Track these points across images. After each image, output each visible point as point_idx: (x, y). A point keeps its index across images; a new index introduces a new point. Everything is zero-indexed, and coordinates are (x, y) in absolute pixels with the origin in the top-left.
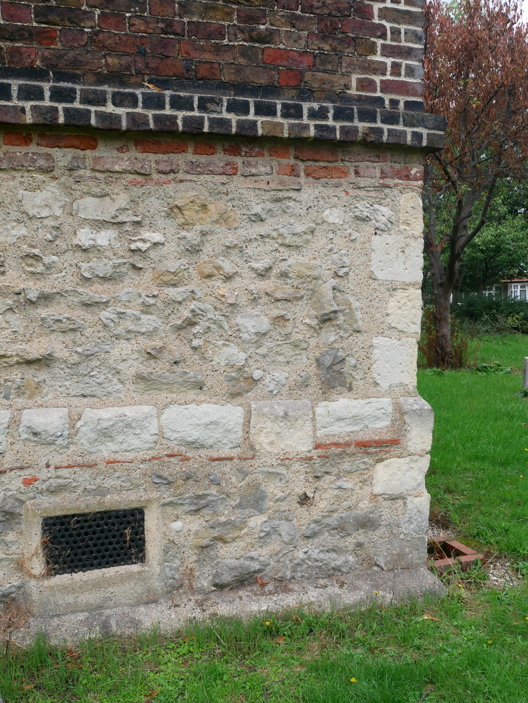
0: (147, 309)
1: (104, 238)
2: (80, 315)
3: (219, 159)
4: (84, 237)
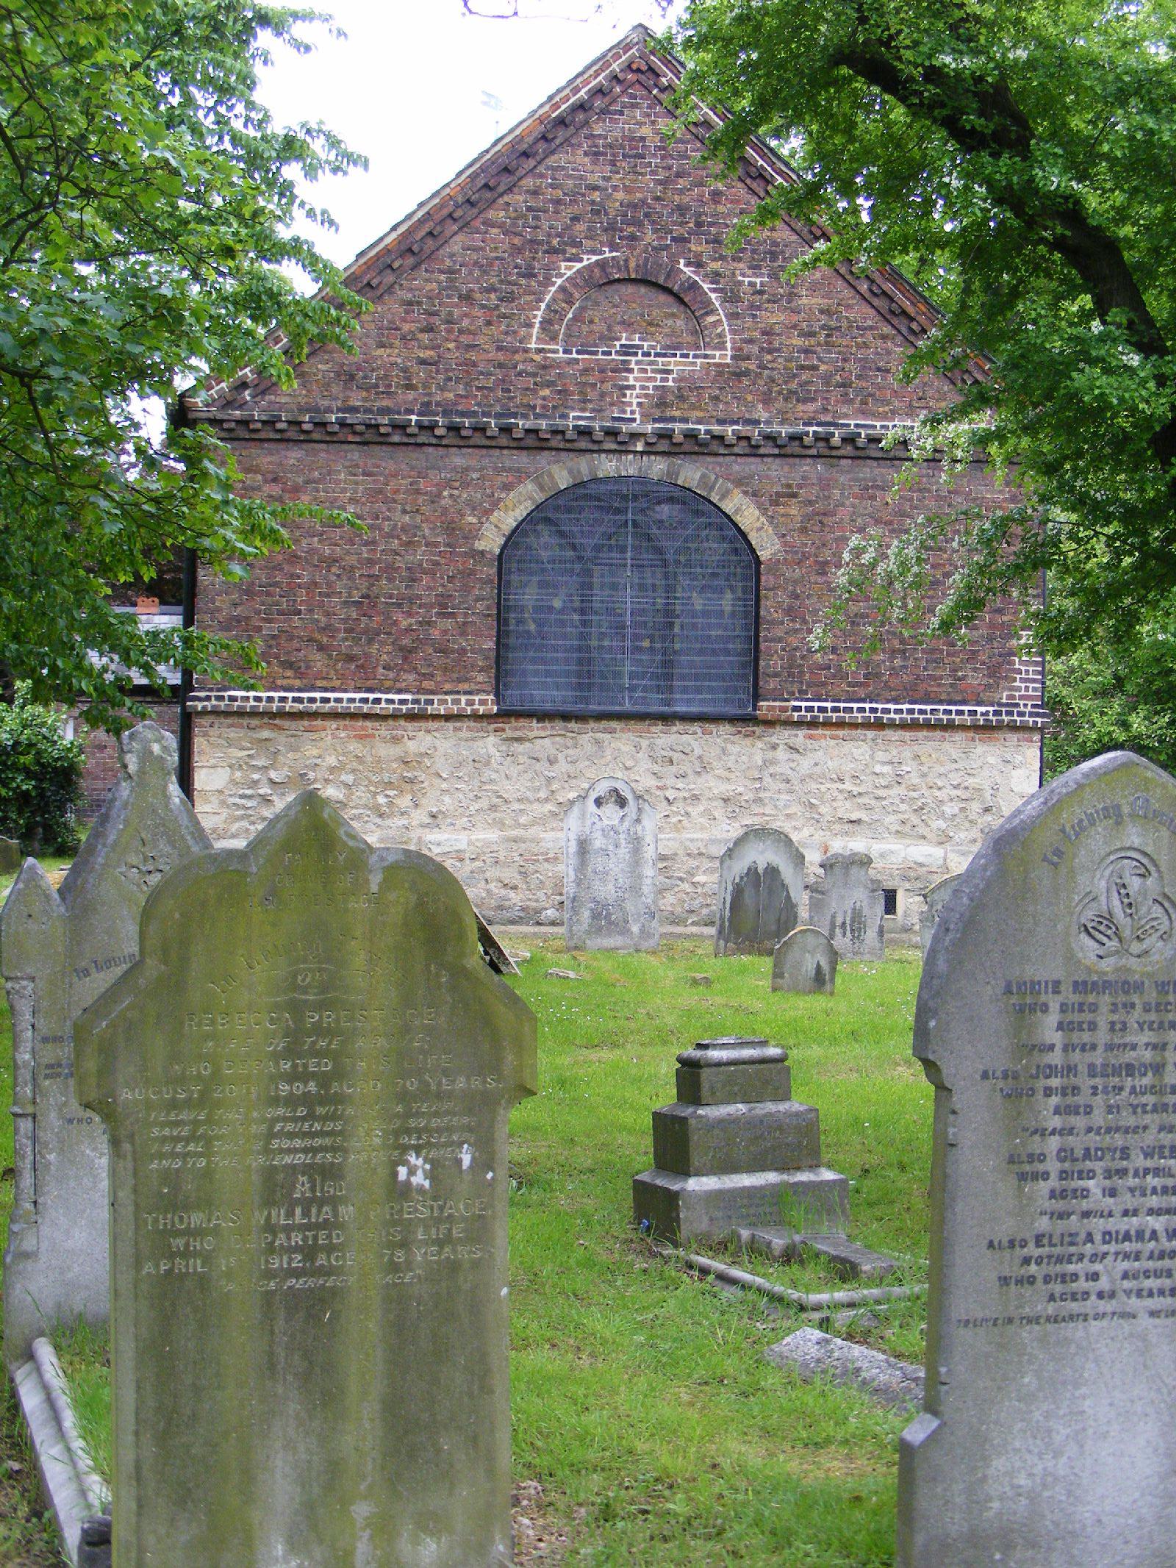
0: (903, 801)
1: (886, 769)
2: (873, 802)
3: (938, 734)
4: (878, 769)
